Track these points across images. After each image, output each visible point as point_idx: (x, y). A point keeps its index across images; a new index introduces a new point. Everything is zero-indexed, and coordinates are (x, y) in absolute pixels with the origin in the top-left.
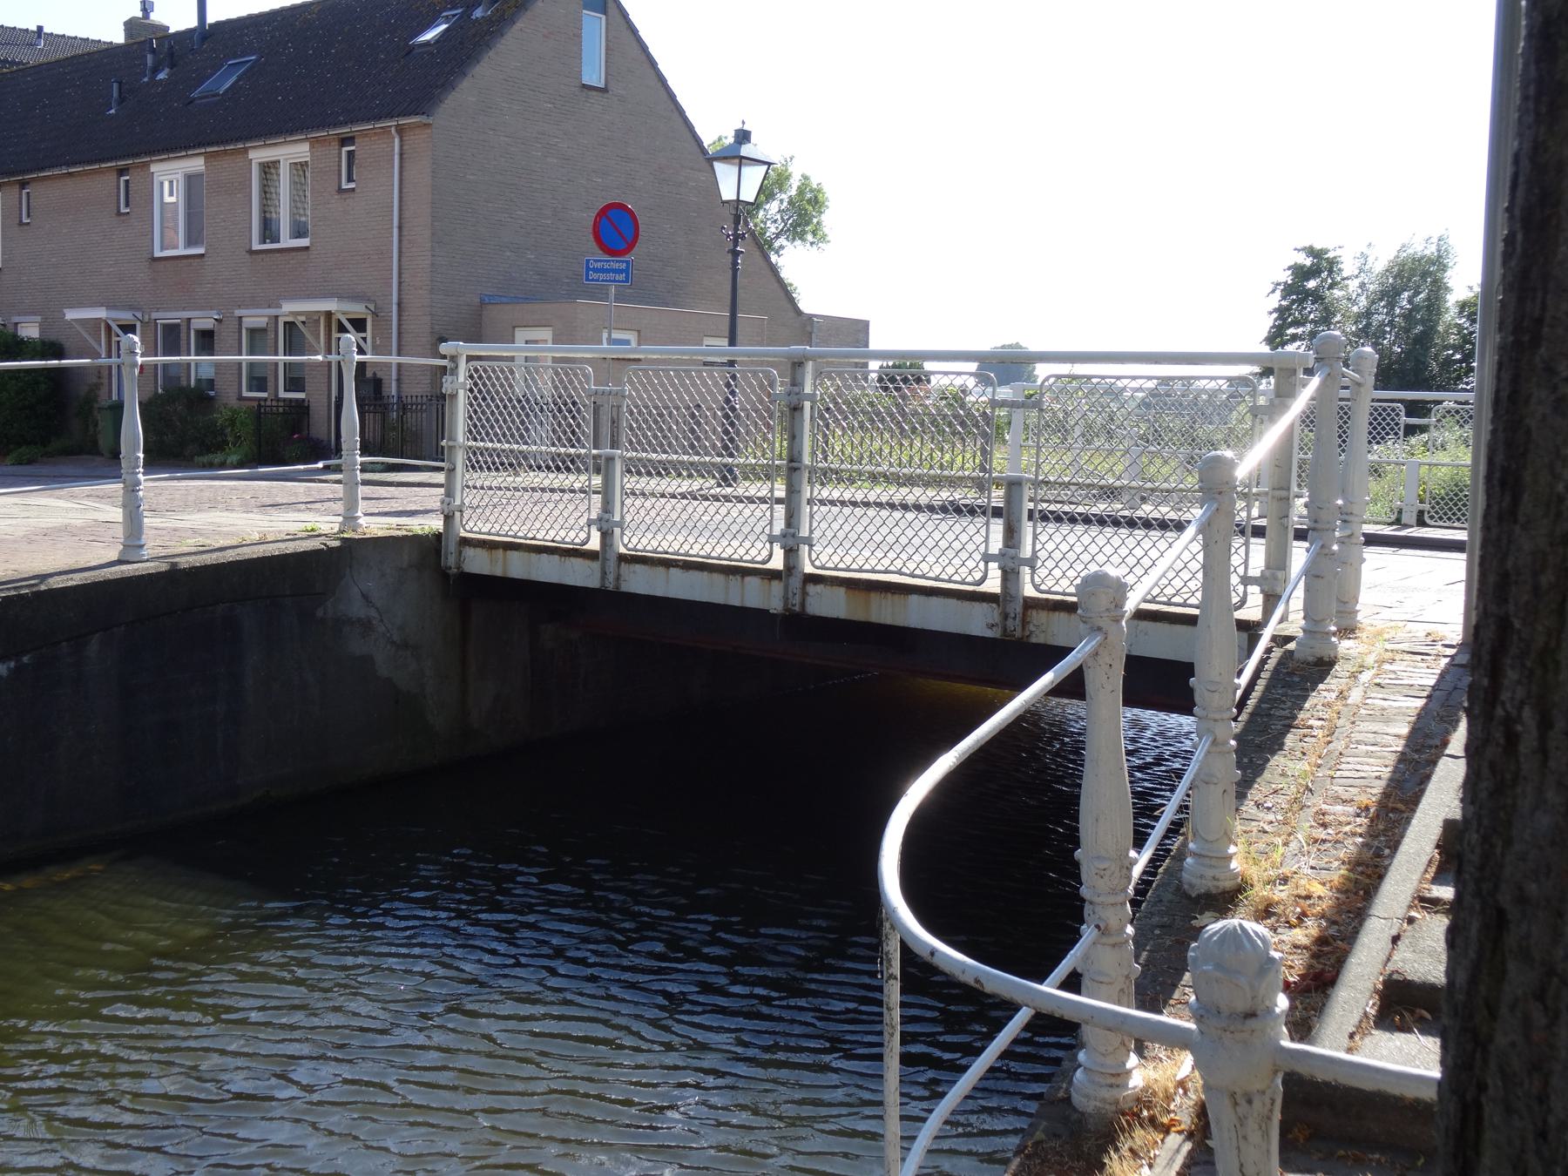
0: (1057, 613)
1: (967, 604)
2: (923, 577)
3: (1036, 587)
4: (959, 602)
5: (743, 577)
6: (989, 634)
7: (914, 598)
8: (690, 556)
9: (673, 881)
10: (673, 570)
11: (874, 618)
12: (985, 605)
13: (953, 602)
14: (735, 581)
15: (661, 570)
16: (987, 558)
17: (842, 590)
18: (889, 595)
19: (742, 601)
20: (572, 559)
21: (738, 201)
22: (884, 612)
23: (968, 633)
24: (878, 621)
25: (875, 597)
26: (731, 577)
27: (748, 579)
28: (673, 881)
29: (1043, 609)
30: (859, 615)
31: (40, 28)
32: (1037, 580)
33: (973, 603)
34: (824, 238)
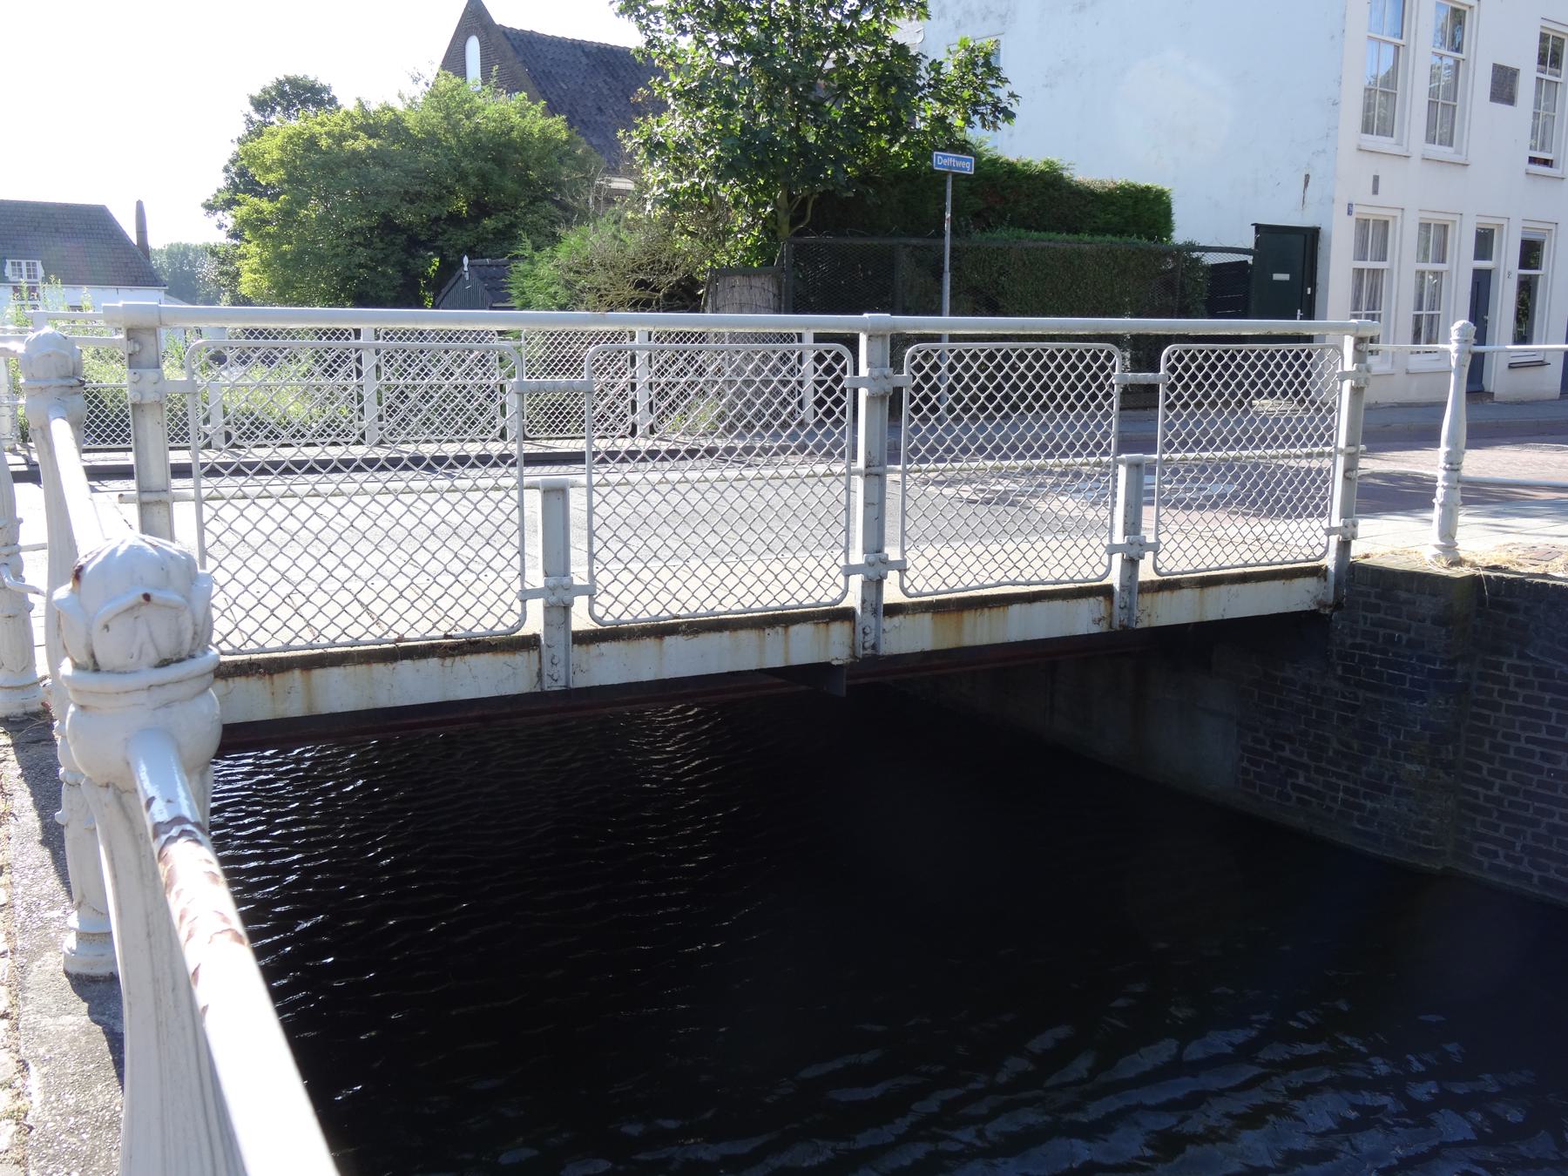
0: (1161, 593)
1: (1073, 603)
2: (1014, 583)
3: (904, 591)
4: (1065, 602)
5: (786, 627)
6: (1095, 629)
7: (1015, 609)
8: (1062, 583)
9: (253, 864)
10: (669, 640)
11: (968, 641)
12: (1091, 600)
13: (1277, 584)
14: (774, 636)
15: (650, 643)
16: (849, 571)
17: (928, 617)
18: (986, 610)
19: (787, 653)
20: (468, 658)
21: (20, 549)
22: (981, 631)
23: (1073, 634)
24: (972, 644)
25: (969, 617)
26: (767, 631)
27: (794, 629)
28: (253, 864)
29: (1148, 592)
30: (948, 642)
31: (21, 521)
32: (907, 583)
33: (1080, 600)
34: (1544, 38)
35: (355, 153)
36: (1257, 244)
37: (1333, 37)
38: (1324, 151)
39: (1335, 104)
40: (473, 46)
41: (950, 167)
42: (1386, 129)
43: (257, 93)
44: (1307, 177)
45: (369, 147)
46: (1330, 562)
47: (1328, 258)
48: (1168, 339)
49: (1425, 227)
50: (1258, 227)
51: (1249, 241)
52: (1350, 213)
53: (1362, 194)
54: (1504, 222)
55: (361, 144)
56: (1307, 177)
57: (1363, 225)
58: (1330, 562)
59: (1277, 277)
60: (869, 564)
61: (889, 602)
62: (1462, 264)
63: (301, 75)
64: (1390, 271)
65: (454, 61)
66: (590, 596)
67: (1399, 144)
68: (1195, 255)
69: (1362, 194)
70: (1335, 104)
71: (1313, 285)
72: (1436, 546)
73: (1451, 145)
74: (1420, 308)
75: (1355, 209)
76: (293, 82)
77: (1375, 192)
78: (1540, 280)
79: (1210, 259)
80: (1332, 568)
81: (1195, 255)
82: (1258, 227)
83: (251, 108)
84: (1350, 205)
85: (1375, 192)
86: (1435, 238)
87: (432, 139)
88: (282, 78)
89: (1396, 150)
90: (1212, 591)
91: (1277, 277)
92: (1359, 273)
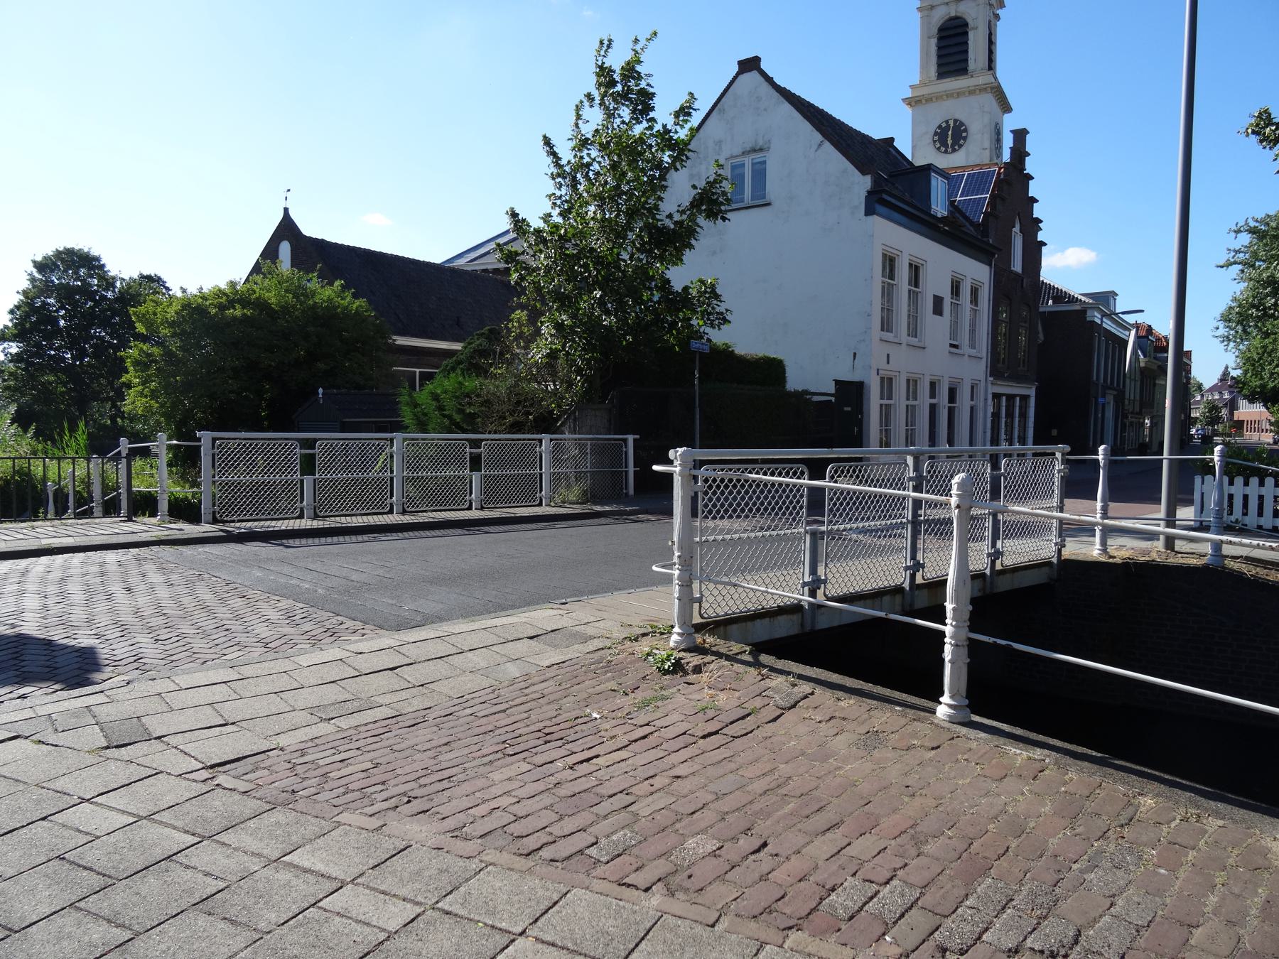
3: (702, 617)
35: (234, 318)
36: (836, 390)
37: (866, 280)
38: (864, 340)
39: (869, 315)
40: (285, 249)
41: (698, 349)
42: (889, 330)
43: (39, 259)
44: (855, 354)
45: (244, 315)
46: (1055, 560)
47: (869, 399)
48: (482, 440)
49: (908, 381)
50: (837, 382)
51: (832, 390)
52: (878, 374)
53: (882, 364)
54: (941, 378)
55: (238, 312)
56: (855, 354)
57: (882, 379)
58: (1055, 560)
59: (846, 409)
60: (813, 581)
61: (1067, 557)
62: (924, 401)
63: (77, 248)
64: (895, 405)
65: (270, 252)
66: (700, 603)
67: (896, 337)
68: (808, 397)
69: (882, 364)
70: (869, 315)
71: (862, 413)
72: (1099, 550)
73: (916, 337)
74: (881, 426)
75: (881, 372)
76: (70, 252)
77: (888, 363)
78: (956, 409)
79: (816, 398)
80: (1056, 562)
81: (808, 397)
82: (837, 382)
83: (35, 271)
84: (878, 370)
85: (888, 363)
86: (912, 384)
87: (286, 309)
88: (61, 249)
89: (920, 344)
90: (1016, 574)
91: (846, 409)
92: (881, 405)
